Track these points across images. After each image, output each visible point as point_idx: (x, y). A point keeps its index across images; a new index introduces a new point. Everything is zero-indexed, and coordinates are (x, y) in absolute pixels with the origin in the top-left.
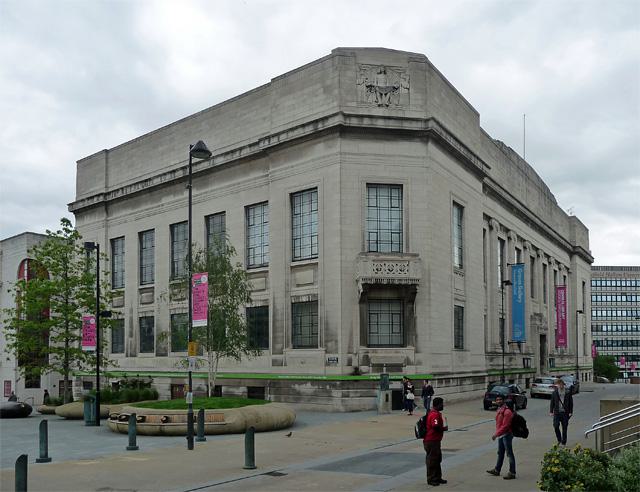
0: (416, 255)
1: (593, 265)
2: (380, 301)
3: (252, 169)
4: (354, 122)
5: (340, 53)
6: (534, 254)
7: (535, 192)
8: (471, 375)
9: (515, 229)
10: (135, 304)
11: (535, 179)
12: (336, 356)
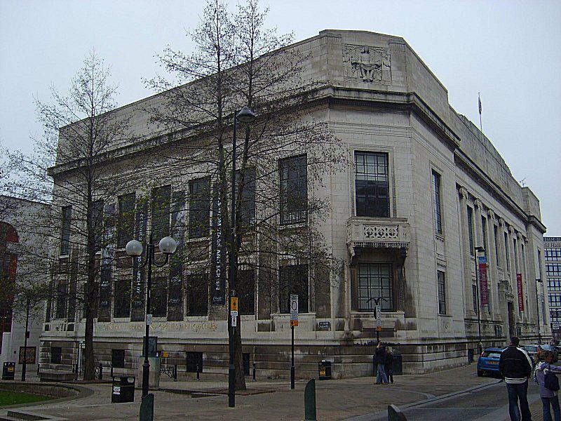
1: (545, 235)
2: (369, 265)
4: (342, 95)
5: (325, 34)
6: (496, 222)
7: (493, 163)
8: (454, 341)
9: (466, 186)
11: (493, 152)
12: (327, 320)
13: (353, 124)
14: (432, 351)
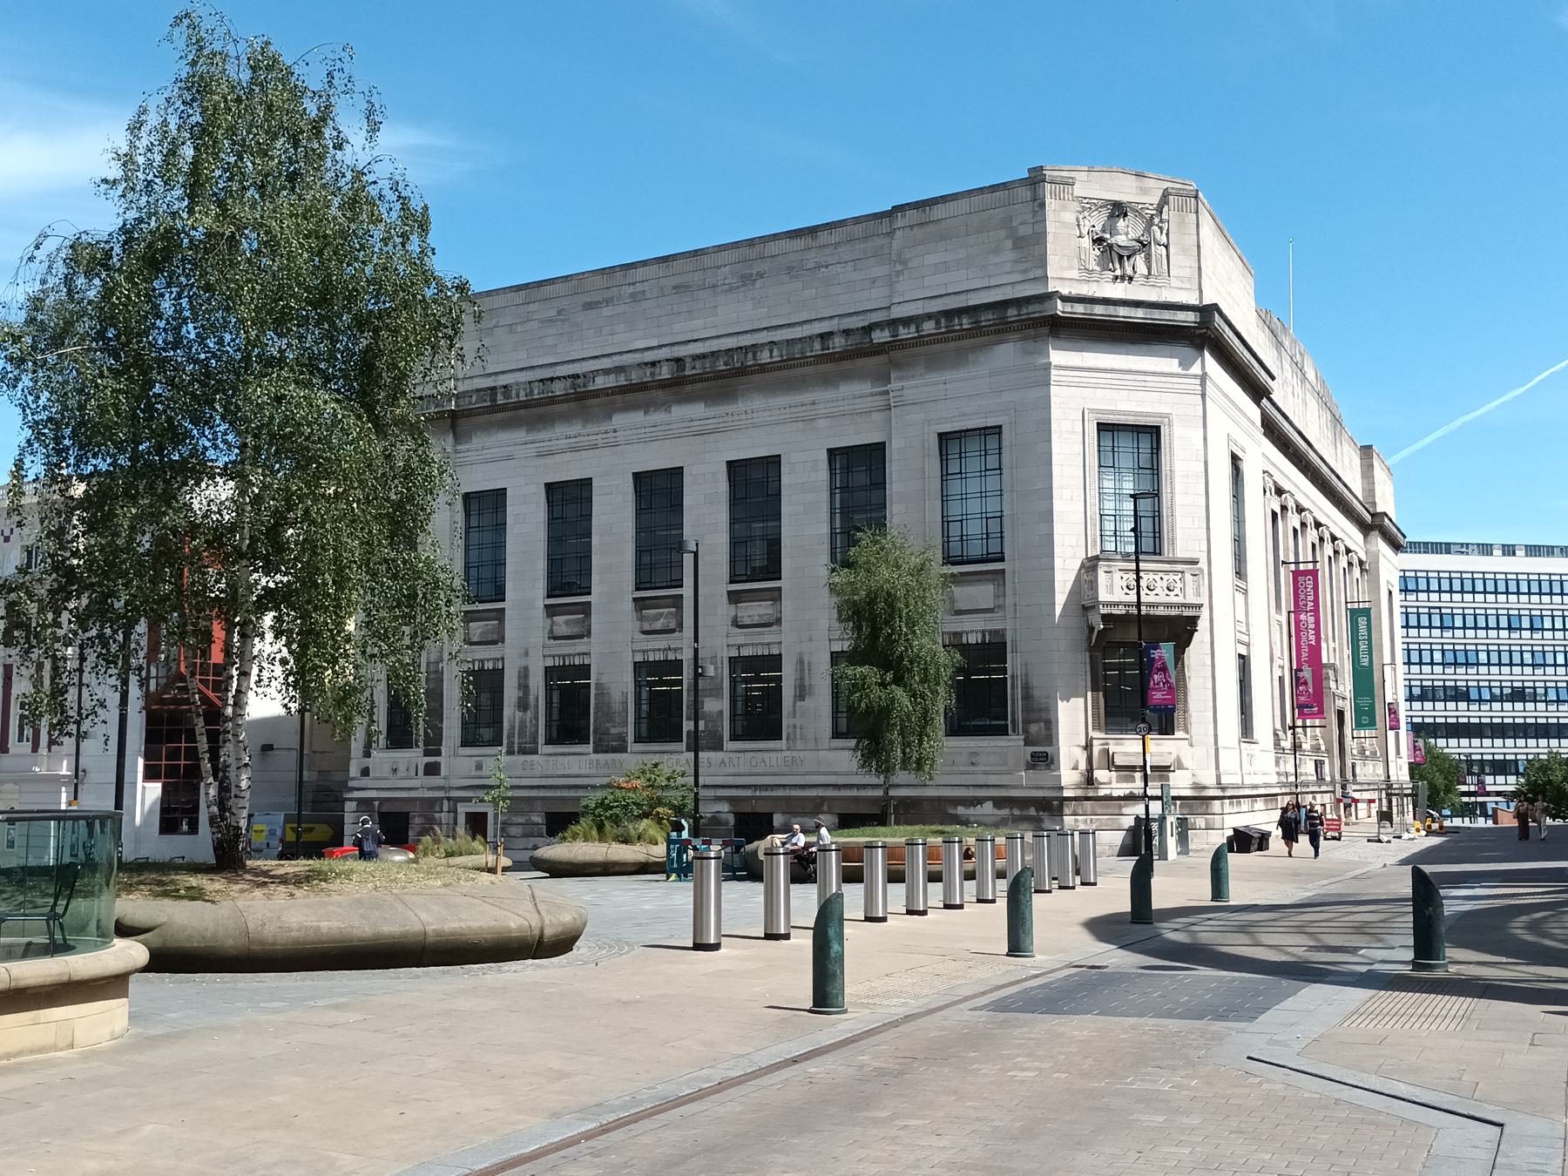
3: (847, 377)
10: (538, 636)
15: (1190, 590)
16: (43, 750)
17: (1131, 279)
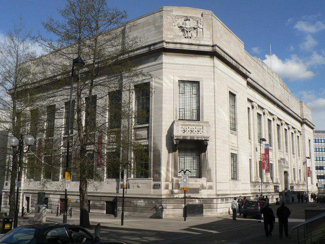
0: (207, 123)
6: (279, 123)
13: (178, 64)
14: (224, 202)
15: (205, 132)
16: (59, 215)
17: (190, 38)
